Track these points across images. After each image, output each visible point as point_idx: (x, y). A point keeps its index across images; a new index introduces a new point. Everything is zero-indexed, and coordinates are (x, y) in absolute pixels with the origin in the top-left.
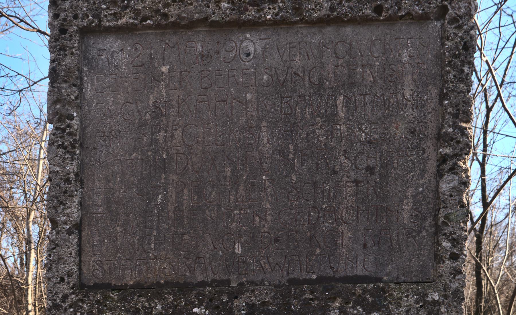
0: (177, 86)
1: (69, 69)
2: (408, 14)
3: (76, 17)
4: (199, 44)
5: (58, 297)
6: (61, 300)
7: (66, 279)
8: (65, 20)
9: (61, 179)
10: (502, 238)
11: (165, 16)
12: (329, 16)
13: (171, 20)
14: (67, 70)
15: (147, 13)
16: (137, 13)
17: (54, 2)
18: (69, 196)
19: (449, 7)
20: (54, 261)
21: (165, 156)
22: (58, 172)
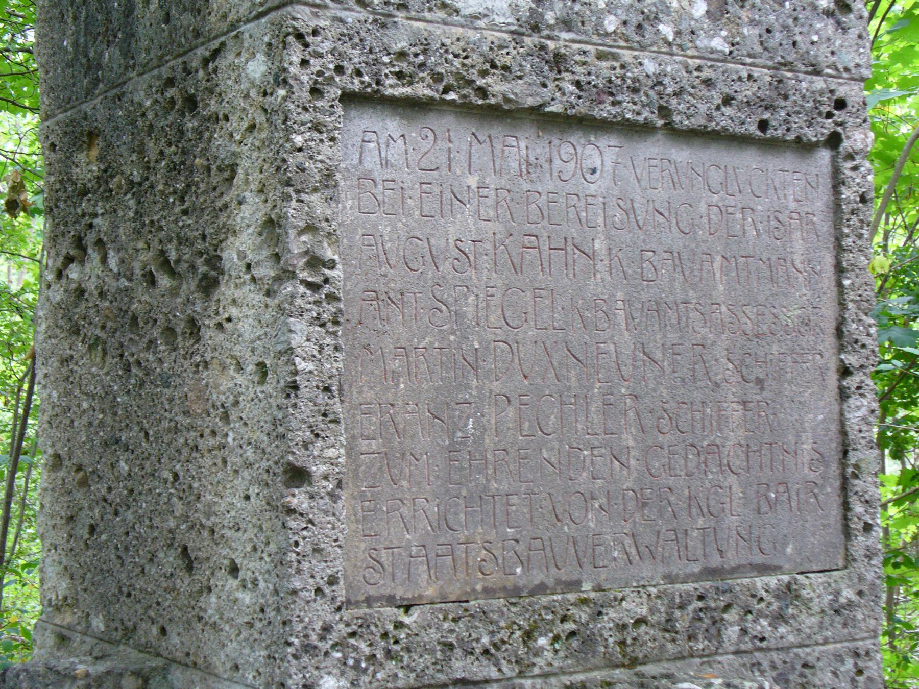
0: (492, 214)
1: (328, 170)
2: (798, 139)
3: (339, 70)
4: (522, 145)
5: (314, 630)
6: (319, 635)
7: (327, 590)
8: (320, 74)
9: (318, 387)
10: (624, 264)
11: (482, 92)
12: (705, 127)
13: (493, 101)
14: (325, 172)
15: (452, 80)
16: (437, 78)
17: (916, 5)
18: (330, 422)
19: (843, 136)
20: (304, 556)
21: (477, 346)
22: (311, 372)
